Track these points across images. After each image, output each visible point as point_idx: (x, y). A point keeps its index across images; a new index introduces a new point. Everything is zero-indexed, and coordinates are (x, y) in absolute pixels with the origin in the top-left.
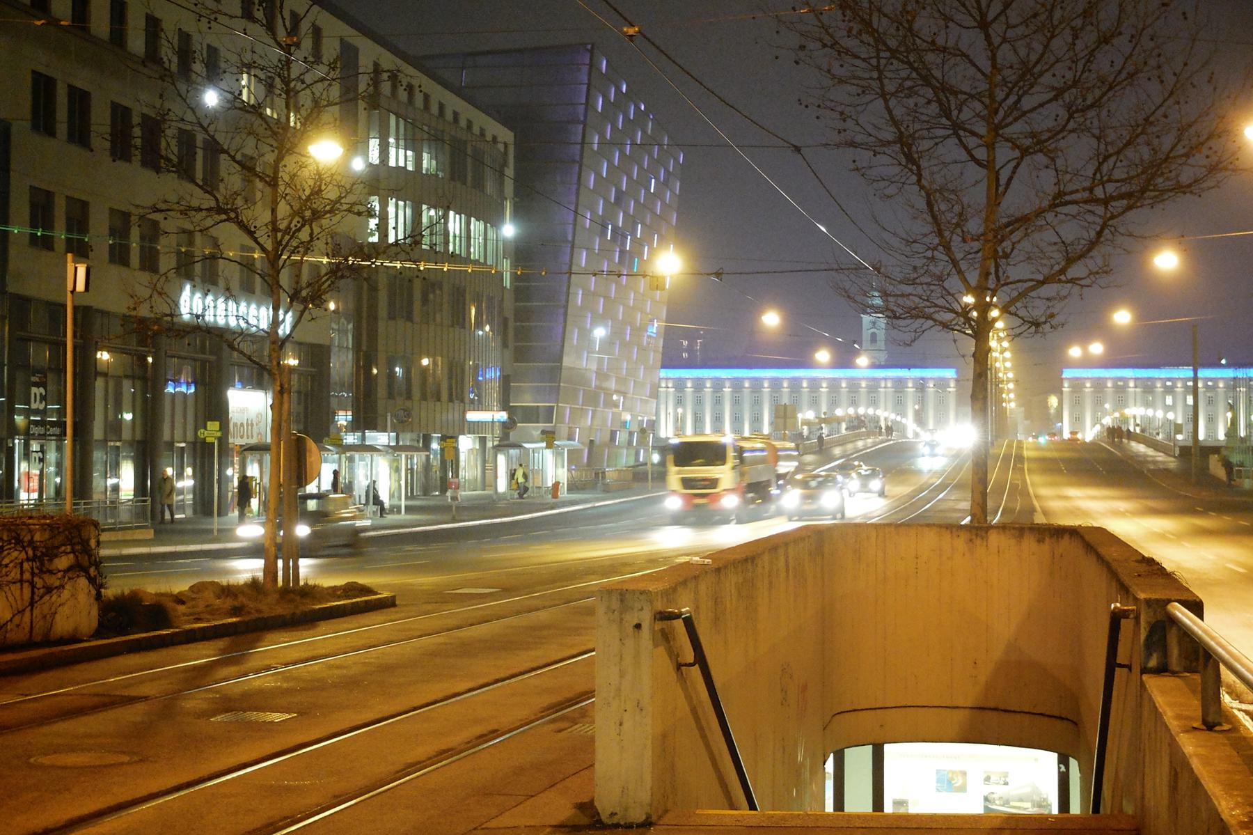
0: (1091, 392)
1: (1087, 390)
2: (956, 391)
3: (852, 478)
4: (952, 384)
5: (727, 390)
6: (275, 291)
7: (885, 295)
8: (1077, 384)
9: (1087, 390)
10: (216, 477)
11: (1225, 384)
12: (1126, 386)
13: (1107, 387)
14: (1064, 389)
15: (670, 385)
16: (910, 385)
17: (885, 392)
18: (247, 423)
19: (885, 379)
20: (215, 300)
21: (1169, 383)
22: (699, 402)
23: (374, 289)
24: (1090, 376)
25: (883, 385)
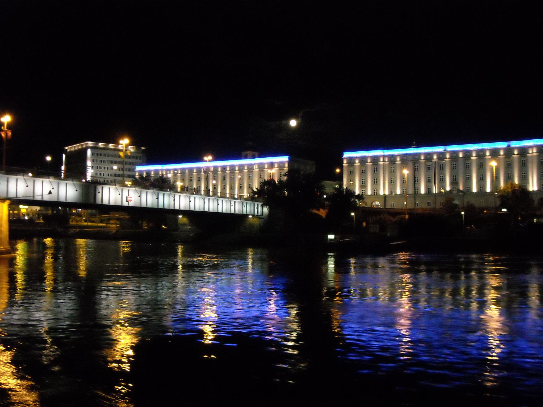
0: (359, 165)
1: (194, 174)
2: (505, 158)
3: (266, 207)
4: (286, 165)
5: (369, 164)
6: (55, 297)
7: (120, 156)
8: (351, 161)
9: (194, 174)
10: (354, 342)
11: (425, 157)
12: (485, 155)
13: (500, 155)
14: (344, 165)
15: (386, 160)
16: (369, 160)
17: (384, 165)
18: (466, 301)
19: (532, 147)
20: (81, 264)
21: (176, 172)
22: (224, 179)
23: (10, 253)
24: (517, 146)
25: (530, 152)
